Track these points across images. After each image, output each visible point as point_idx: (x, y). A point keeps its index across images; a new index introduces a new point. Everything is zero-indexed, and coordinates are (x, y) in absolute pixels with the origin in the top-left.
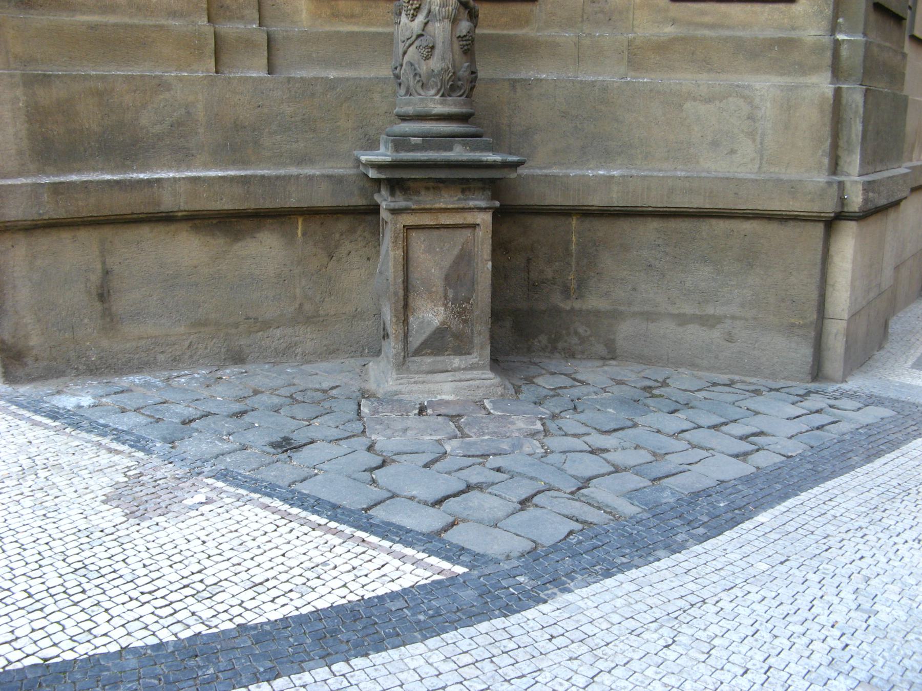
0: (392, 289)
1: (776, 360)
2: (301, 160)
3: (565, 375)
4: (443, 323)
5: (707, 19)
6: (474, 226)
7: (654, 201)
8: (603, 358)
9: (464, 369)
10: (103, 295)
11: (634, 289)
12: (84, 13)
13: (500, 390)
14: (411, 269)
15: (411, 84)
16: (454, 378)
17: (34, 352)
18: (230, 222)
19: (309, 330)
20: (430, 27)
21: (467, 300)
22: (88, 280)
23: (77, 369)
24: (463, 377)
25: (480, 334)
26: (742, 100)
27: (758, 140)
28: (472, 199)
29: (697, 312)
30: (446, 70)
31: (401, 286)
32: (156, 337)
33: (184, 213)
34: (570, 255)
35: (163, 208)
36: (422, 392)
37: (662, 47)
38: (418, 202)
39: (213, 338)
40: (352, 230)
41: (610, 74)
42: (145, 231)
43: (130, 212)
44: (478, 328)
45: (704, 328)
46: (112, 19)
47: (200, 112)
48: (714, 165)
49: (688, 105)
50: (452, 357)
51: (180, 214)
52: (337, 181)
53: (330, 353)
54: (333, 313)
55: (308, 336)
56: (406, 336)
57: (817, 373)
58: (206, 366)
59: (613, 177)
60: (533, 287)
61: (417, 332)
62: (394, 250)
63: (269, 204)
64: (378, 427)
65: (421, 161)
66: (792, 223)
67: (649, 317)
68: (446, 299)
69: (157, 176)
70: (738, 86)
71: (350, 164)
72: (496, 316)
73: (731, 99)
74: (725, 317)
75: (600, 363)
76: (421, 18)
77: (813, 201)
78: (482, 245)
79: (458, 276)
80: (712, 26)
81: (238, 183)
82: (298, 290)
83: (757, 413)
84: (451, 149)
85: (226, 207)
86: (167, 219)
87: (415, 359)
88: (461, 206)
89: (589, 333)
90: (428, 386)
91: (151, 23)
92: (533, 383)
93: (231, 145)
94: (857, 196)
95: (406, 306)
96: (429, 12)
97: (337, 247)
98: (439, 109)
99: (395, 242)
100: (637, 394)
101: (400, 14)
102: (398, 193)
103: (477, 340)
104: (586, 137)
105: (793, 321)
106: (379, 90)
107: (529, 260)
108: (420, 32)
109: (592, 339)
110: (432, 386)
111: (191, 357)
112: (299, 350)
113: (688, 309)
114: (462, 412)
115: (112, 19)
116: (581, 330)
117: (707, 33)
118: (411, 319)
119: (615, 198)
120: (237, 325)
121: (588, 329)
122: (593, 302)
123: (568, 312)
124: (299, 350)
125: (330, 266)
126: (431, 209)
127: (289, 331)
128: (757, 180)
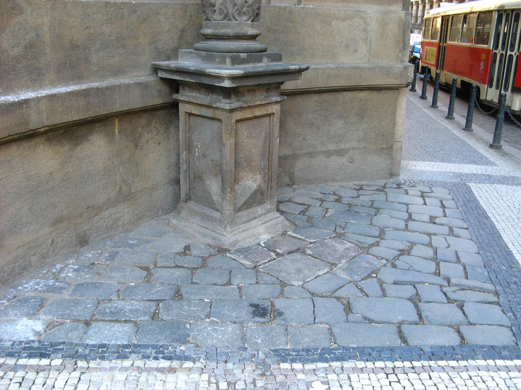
1: (374, 169)
2: (117, 72)
4: (259, 186)
6: (269, 115)
8: (288, 185)
9: (265, 214)
15: (230, 12)
19: (126, 206)
24: (266, 219)
26: (361, 19)
27: (368, 43)
29: (336, 149)
33: (46, 129)
35: (32, 126)
39: (67, 230)
40: (149, 124)
43: (7, 135)
45: (339, 157)
47: (47, 37)
48: (347, 60)
49: (334, 23)
50: (256, 207)
51: (42, 130)
53: (139, 220)
61: (240, 195)
66: (383, 91)
67: (312, 155)
70: (359, 11)
71: (148, 71)
73: (355, 19)
74: (350, 149)
77: (397, 78)
81: (81, 96)
84: (260, 61)
85: (74, 119)
86: (29, 136)
93: (69, 63)
94: (411, 74)
97: (140, 138)
102: (233, 96)
104: (281, 44)
105: (382, 146)
106: (164, 13)
109: (282, 174)
111: (54, 250)
112: (120, 223)
113: (331, 147)
120: (81, 215)
121: (280, 169)
127: (114, 210)
128: (370, 68)
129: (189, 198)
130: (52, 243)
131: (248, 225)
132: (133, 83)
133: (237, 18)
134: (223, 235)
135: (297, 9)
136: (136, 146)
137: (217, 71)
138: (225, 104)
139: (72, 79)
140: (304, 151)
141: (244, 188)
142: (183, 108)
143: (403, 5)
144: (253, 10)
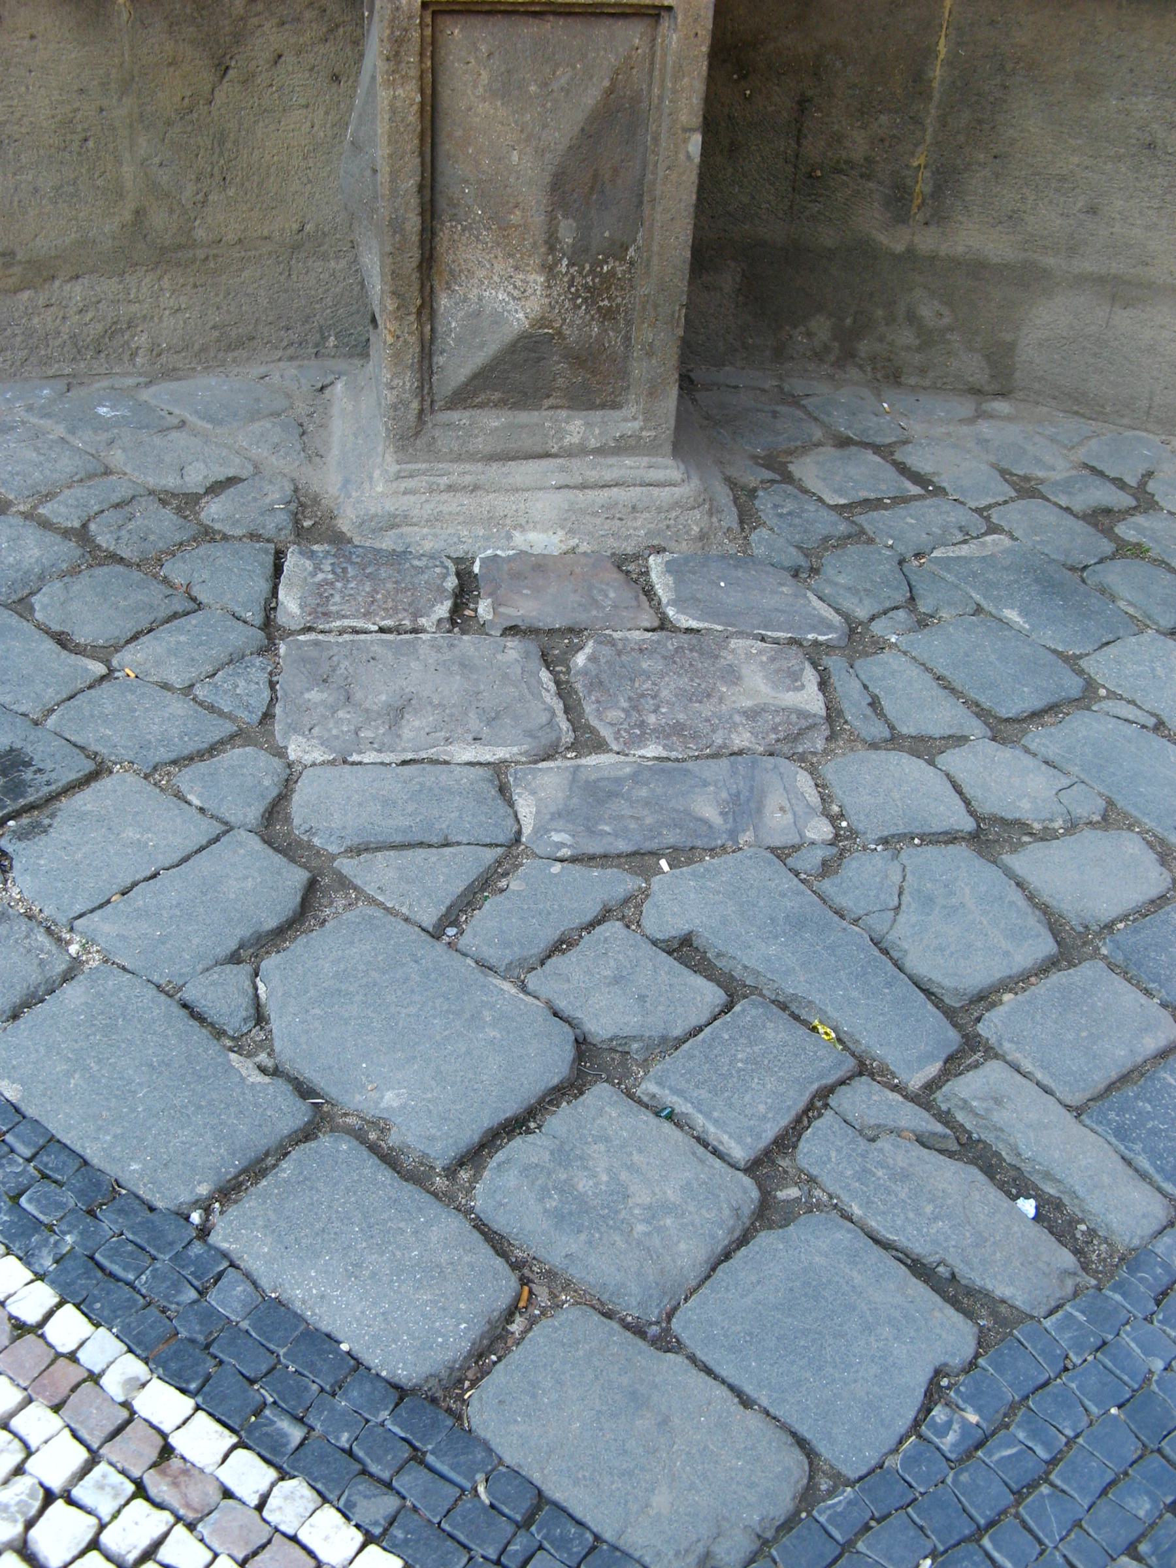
0: (384, 210)
3: (877, 449)
4: (542, 321)
8: (976, 392)
9: (600, 451)
11: (1092, 210)
13: (696, 521)
14: (446, 147)
16: (563, 479)
19: (166, 283)
21: (618, 250)
24: (593, 475)
25: (650, 354)
31: (414, 201)
34: (925, 95)
44: (645, 334)
50: (563, 413)
53: (229, 348)
54: (231, 237)
55: (167, 300)
56: (427, 350)
60: (810, 180)
61: (459, 340)
62: (391, 84)
64: (314, 695)
67: (1120, 290)
68: (551, 249)
72: (703, 258)
75: (966, 407)
78: (676, 78)
79: (595, 176)
87: (455, 416)
89: (946, 320)
92: (788, 478)
95: (428, 261)
97: (238, 38)
99: (394, 58)
100: (1084, 543)
103: (639, 369)
107: (803, 103)
109: (954, 337)
110: (503, 503)
112: (142, 340)
114: (581, 618)
116: (926, 312)
118: (444, 301)
121: (945, 311)
122: (972, 237)
123: (898, 258)
124: (142, 340)
125: (220, 97)
127: (110, 286)
131: (494, 471)
140: (1088, 266)
141: (478, 314)
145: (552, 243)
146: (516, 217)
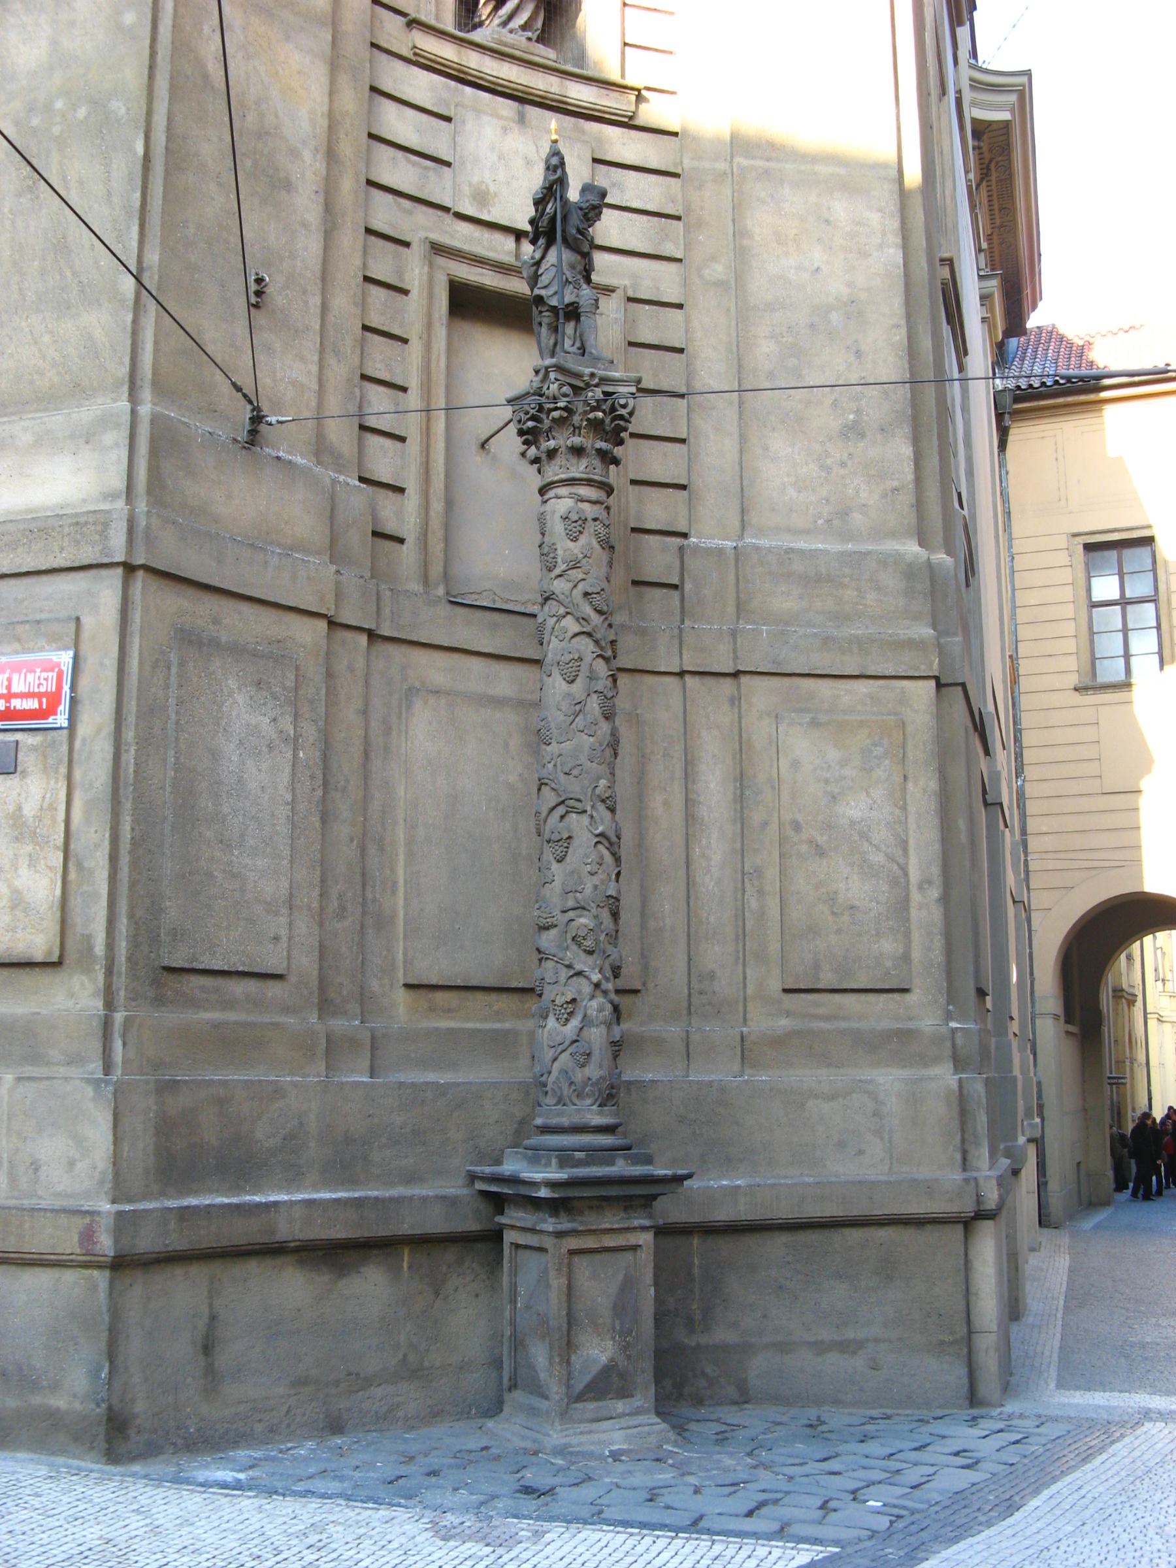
2: (411, 1178)
4: (612, 1360)
5: (822, 1011)
6: (634, 1248)
7: (784, 1211)
8: (736, 1403)
10: (207, 1349)
11: (765, 1316)
12: (206, 1010)
15: (566, 1093)
17: (138, 1421)
18: (334, 1254)
19: (412, 1387)
20: (585, 1032)
22: (195, 1328)
23: (174, 1444)
28: (636, 1218)
30: (603, 1078)
32: (255, 1400)
33: (298, 1243)
36: (593, 1443)
37: (779, 1042)
38: (581, 1223)
39: (312, 1400)
41: (720, 1072)
42: (252, 1266)
45: (846, 1356)
46: (231, 1016)
48: (843, 1168)
49: (810, 1104)
51: (293, 1244)
52: (450, 1202)
54: (438, 1364)
57: (973, 1398)
58: (310, 1438)
59: (739, 1187)
63: (382, 1232)
65: (599, 1178)
66: (929, 1227)
67: (783, 1347)
69: (272, 1199)
70: (860, 1081)
71: (460, 1182)
73: (854, 1095)
74: (867, 1340)
75: (735, 1408)
76: (575, 1022)
77: (951, 1200)
79: (623, 1307)
80: (827, 1018)
82: (402, 1337)
83: (944, 1437)
84: (613, 1164)
85: (339, 1236)
86: (273, 1250)
87: (578, 1405)
88: (626, 1226)
90: (596, 1436)
91: (268, 1020)
96: (585, 1016)
98: (597, 1120)
101: (547, 1016)
102: (562, 1214)
105: (942, 1337)
108: (575, 1038)
109: (721, 1380)
110: (604, 1437)
111: (288, 1426)
112: (400, 1414)
113: (826, 1334)
115: (231, 1016)
116: (708, 1370)
117: (823, 1025)
118: (573, 1358)
119: (743, 1211)
120: (337, 1383)
122: (722, 1335)
124: (400, 1414)
126: (595, 1231)
129: (513, 1386)
130: (288, 1412)
131: (595, 1426)
132: (435, 1194)
133: (576, 1101)
134: (549, 1435)
135: (735, 1084)
136: (437, 1294)
137: (531, 1175)
138: (549, 1224)
139: (342, 1184)
142: (509, 1237)
143: (955, 1065)
144: (600, 1090)
145: (614, 1329)
146: (601, 1321)
